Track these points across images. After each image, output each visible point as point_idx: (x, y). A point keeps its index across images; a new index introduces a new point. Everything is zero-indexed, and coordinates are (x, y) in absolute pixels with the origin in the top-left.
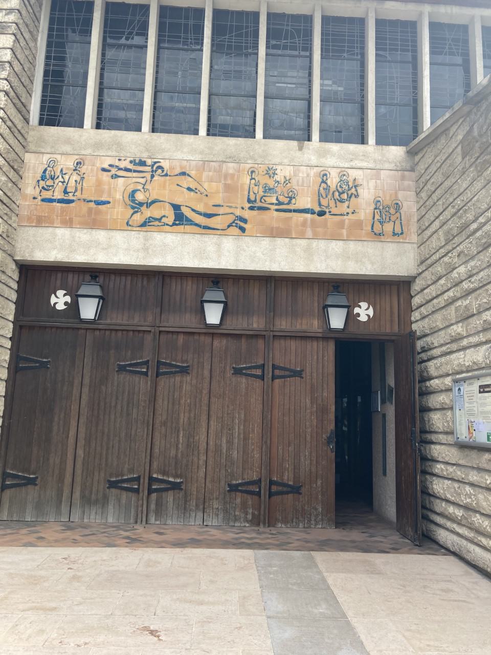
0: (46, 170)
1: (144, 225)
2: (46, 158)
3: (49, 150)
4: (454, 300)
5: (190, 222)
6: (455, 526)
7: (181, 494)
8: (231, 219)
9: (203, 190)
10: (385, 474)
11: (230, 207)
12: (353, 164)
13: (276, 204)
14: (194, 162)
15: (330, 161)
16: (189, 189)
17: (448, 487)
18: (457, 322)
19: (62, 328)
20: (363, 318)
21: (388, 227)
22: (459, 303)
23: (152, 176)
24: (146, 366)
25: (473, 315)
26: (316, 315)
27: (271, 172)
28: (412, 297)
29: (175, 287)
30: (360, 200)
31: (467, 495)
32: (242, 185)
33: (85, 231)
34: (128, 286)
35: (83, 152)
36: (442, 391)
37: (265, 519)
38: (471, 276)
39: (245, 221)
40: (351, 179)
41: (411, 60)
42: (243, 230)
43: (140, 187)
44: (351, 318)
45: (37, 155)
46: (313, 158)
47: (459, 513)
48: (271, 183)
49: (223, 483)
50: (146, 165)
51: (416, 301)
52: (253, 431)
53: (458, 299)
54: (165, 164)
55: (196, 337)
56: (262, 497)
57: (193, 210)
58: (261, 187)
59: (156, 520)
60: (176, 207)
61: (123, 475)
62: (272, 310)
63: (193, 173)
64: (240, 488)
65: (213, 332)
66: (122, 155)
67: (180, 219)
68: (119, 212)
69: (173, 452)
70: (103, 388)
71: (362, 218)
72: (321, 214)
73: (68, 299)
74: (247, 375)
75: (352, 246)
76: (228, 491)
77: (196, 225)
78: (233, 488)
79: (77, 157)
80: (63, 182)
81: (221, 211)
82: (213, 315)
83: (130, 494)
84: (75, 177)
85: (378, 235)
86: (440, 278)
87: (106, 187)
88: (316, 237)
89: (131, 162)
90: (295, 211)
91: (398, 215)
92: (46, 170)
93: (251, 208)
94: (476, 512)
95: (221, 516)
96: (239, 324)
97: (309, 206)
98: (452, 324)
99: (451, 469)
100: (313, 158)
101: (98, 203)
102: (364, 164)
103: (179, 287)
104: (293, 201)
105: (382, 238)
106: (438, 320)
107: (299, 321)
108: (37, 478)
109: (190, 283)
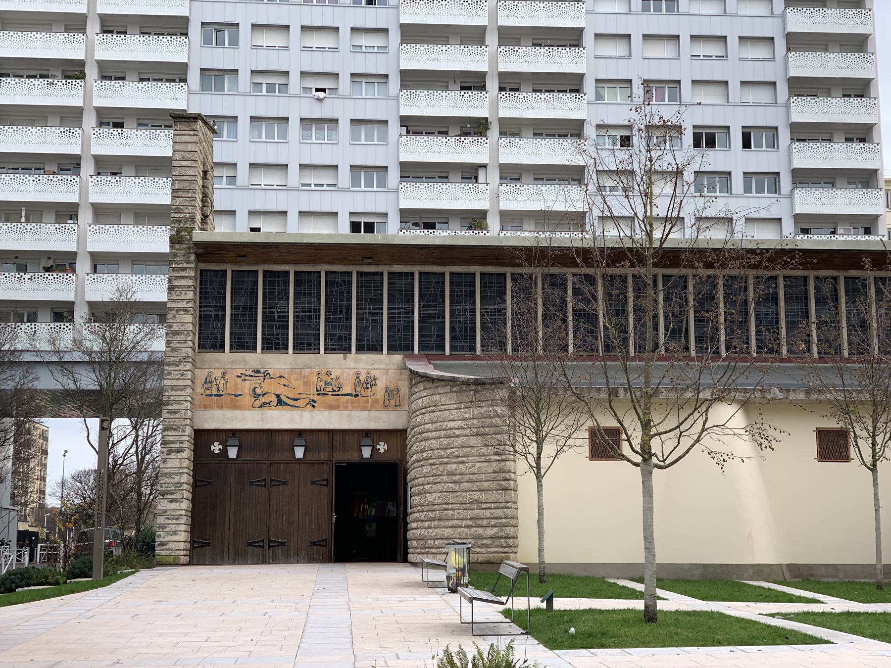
1: (261, 406)
5: (285, 403)
12: (374, 366)
21: (393, 402)
39: (315, 402)
40: (372, 376)
60: (278, 396)
63: (286, 376)
67: (280, 402)
68: (247, 399)
72: (356, 396)
73: (221, 447)
75: (373, 413)
78: (313, 544)
81: (302, 396)
82: (299, 453)
84: (223, 381)
85: (387, 407)
93: (318, 394)
96: (313, 457)
101: (236, 396)
102: (380, 366)
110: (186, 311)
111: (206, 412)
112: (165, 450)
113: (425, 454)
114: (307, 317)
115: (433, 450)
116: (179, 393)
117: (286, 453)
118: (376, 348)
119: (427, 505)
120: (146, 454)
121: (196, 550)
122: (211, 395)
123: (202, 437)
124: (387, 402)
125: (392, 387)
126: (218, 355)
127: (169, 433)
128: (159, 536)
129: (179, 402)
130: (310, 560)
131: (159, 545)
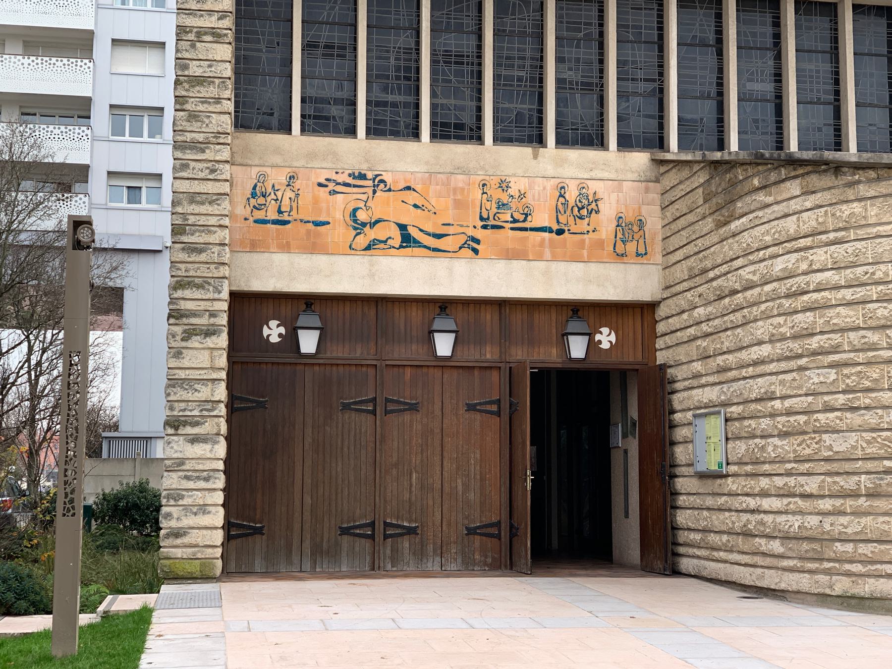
0: (255, 186)
1: (368, 248)
2: (255, 171)
3: (257, 162)
4: (696, 338)
5: (416, 242)
6: (695, 550)
7: (417, 540)
8: (462, 239)
9: (430, 208)
10: (627, 516)
11: (462, 226)
12: (593, 174)
13: (511, 222)
14: (419, 175)
15: (568, 171)
16: (415, 206)
17: (690, 516)
18: (698, 360)
19: (278, 363)
20: (605, 345)
21: (631, 247)
22: (699, 342)
23: (374, 192)
24: (371, 404)
25: (710, 357)
26: (555, 342)
27: (504, 185)
28: (657, 322)
29: (399, 315)
30: (600, 215)
31: (705, 519)
32: (473, 201)
33: (305, 256)
34: (348, 315)
35: (295, 164)
36: (685, 424)
37: (506, 562)
38: (708, 320)
39: (478, 242)
40: (591, 193)
41: (656, 40)
42: (476, 251)
43: (362, 205)
44: (592, 346)
45: (244, 168)
46: (549, 167)
47: (697, 537)
48: (505, 199)
49: (460, 526)
50: (366, 179)
51: (661, 328)
52: (490, 471)
53: (698, 338)
54: (386, 177)
55: (425, 370)
56: (503, 540)
57: (421, 230)
58: (493, 202)
59: (392, 567)
60: (403, 227)
61: (355, 521)
62: (505, 337)
63: (418, 188)
64: (478, 531)
65: (443, 364)
66: (339, 167)
67: (407, 240)
68: (340, 232)
69: (407, 496)
70: (328, 428)
71: (604, 237)
72: (560, 232)
73: (282, 330)
74: (479, 411)
75: (593, 267)
76: (466, 534)
77: (425, 247)
78: (471, 532)
79: (289, 170)
80: (276, 200)
81: (450, 230)
82: (444, 345)
83: (363, 540)
84: (289, 194)
86: (683, 312)
87: (324, 205)
88: (554, 259)
89: (350, 175)
90: (532, 229)
91: (641, 232)
92: (255, 186)
93: (485, 227)
94: (711, 531)
95: (459, 560)
96: (471, 355)
97: (546, 224)
98: (693, 361)
99: (692, 498)
100: (549, 167)
101: (317, 224)
102: (606, 175)
103: (403, 314)
104: (529, 218)
105: (625, 259)
106: (681, 354)
107: (536, 350)
108: (263, 527)
109: (414, 309)
110: (217, 36)
111: (255, 256)
112: (178, 330)
113: (814, 343)
114: (457, 67)
115: (842, 330)
116: (203, 209)
117: (414, 347)
118: (594, 139)
119: (827, 460)
120: (41, 374)
121: (233, 543)
122: (264, 222)
123: (247, 307)
124: (620, 245)
125: (630, 216)
126: (279, 139)
127: (187, 293)
128: (169, 515)
129: (206, 229)
130: (470, 566)
131: (168, 536)
